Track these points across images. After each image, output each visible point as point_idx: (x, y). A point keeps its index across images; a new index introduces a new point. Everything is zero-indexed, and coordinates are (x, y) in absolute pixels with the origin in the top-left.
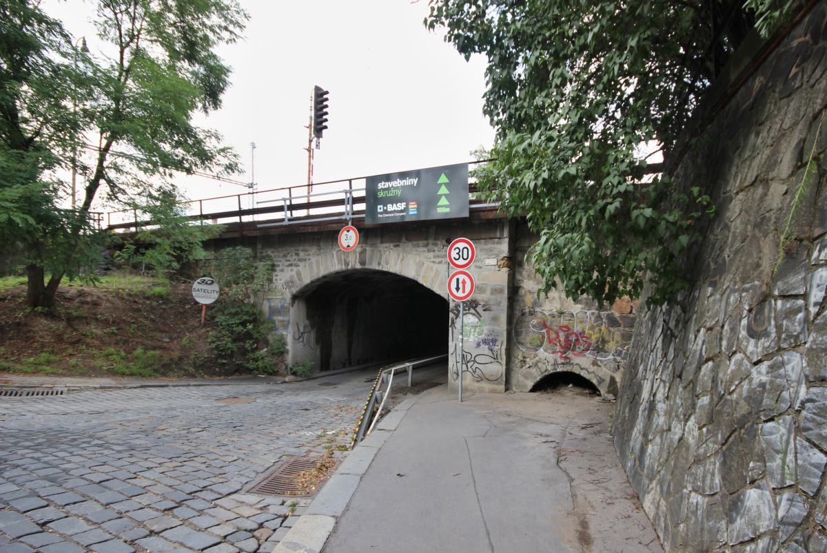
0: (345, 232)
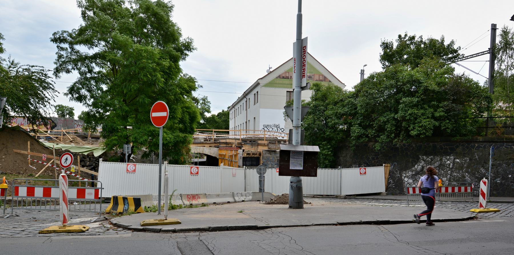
0: (107, 210)
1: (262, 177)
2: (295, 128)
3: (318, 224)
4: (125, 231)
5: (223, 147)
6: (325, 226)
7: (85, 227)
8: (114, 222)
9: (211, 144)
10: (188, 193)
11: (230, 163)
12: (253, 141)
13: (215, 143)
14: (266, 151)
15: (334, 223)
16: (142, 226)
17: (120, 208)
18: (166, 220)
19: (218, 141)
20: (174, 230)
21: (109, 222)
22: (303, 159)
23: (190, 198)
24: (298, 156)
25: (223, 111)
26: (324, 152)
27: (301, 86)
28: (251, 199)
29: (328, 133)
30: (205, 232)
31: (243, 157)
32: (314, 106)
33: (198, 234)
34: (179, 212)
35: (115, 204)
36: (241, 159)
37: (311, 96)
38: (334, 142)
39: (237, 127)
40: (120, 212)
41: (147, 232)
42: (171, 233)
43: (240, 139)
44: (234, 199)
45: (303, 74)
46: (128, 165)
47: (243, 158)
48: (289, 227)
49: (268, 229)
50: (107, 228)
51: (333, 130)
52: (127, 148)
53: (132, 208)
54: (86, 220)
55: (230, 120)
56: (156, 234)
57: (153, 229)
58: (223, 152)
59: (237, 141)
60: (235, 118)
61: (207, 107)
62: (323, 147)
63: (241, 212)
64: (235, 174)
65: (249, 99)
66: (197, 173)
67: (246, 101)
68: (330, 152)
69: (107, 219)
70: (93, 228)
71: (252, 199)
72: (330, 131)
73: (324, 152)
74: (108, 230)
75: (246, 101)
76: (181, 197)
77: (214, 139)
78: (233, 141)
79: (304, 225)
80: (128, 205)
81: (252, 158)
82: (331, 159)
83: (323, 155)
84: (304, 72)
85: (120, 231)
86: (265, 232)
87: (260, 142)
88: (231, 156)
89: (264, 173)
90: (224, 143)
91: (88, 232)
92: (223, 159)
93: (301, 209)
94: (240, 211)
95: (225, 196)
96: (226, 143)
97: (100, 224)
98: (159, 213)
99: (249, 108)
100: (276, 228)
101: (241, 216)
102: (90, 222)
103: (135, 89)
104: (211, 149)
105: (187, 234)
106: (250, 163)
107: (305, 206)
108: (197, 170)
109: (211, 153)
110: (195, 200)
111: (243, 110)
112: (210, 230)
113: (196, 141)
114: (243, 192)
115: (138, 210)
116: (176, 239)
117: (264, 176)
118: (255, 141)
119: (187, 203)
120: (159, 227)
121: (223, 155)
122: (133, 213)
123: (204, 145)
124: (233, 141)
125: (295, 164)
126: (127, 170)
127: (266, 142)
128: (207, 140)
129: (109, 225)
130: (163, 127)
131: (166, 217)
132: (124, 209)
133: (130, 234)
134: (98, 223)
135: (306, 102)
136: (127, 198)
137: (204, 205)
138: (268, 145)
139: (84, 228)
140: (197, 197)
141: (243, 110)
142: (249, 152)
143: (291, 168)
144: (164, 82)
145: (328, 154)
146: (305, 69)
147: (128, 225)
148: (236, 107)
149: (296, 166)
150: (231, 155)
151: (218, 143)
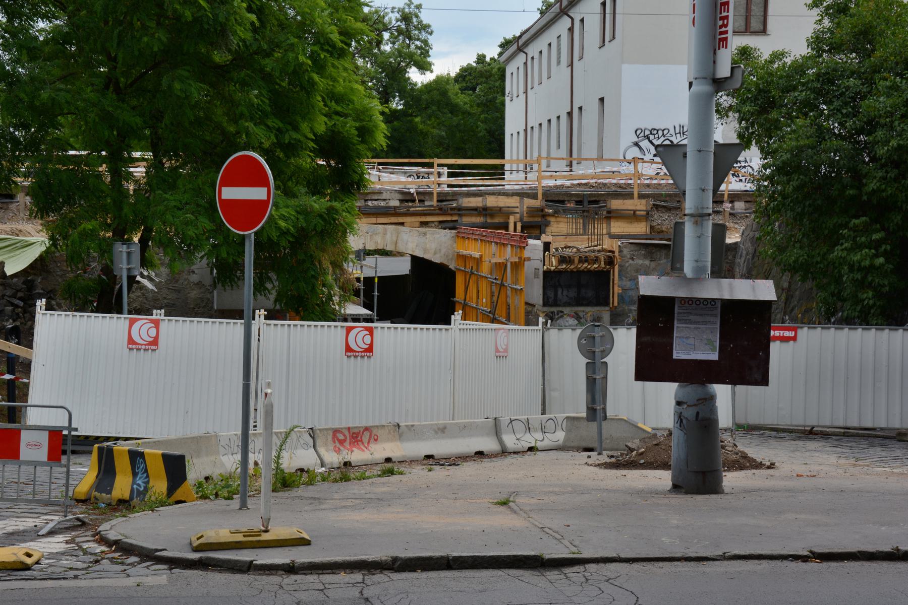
1: (598, 364)
2: (693, 219)
3: (743, 553)
4: (147, 567)
5: (474, 225)
6: (764, 562)
7: (30, 552)
8: (112, 536)
9: (425, 215)
10: (337, 426)
11: (495, 290)
12: (591, 202)
13: (441, 209)
14: (632, 247)
15: (800, 553)
16: (196, 550)
17: (122, 486)
18: (266, 531)
20: (288, 565)
21: (93, 536)
22: (718, 326)
23: (341, 442)
24: (701, 315)
25: (481, 59)
26: (856, 257)
27: (714, 74)
28: (561, 442)
29: (872, 185)
30: (381, 573)
31: (544, 272)
32: (818, 75)
33: (361, 580)
34: (306, 498)
35: (104, 471)
36: (536, 276)
37: (809, 33)
38: (897, 218)
39: (536, 130)
40: (121, 497)
41: (213, 571)
42: (281, 576)
43: (540, 196)
44: (501, 442)
45: (721, 33)
46: (132, 322)
47: (547, 274)
48: (645, 564)
49: (576, 568)
50: (91, 554)
51: (892, 174)
52: (125, 256)
53: (160, 485)
54: (22, 528)
55: (507, 99)
56: (238, 577)
57: (229, 561)
58: (473, 250)
59: (529, 202)
60: (526, 92)
61: (420, 48)
62: (855, 237)
63: (504, 503)
64: (506, 351)
65: (582, 21)
66: (370, 349)
67: (571, 30)
68: (881, 260)
69: (83, 524)
70: (50, 554)
71: (566, 440)
72: (880, 174)
73: (856, 257)
74: (97, 562)
75: (571, 30)
76: (313, 438)
77: (439, 194)
78: (513, 202)
79: (693, 555)
80: (148, 476)
81: (580, 273)
82: (884, 286)
83: (851, 268)
84: (724, 29)
85: (132, 565)
86: (562, 576)
87: (616, 204)
88: (502, 267)
89: (606, 353)
90: (475, 209)
91: (41, 570)
92: (472, 273)
93: (714, 496)
94: (502, 497)
95: (465, 430)
96: (484, 211)
97: (67, 542)
98: (243, 505)
99: (581, 58)
100: (602, 565)
101: (504, 520)
102: (34, 534)
103: (156, 49)
104: (425, 234)
105: (328, 578)
106: (573, 293)
107: (731, 479)
108: (368, 340)
109: (425, 251)
110: (360, 449)
111: (559, 63)
112: (396, 565)
113: (370, 203)
114: (536, 417)
115: (179, 494)
116: (297, 594)
117: (606, 363)
118: (596, 202)
119: (333, 458)
120: (244, 556)
121: (471, 257)
122: (163, 504)
123: (401, 220)
124: (513, 202)
125: (691, 341)
126: (131, 341)
127: (640, 205)
128: (413, 201)
129: (96, 545)
130: (256, 233)
131: (266, 522)
132: (132, 490)
133: (165, 577)
134: (60, 538)
135: (788, 60)
136: (141, 455)
137: (389, 467)
138: (647, 216)
139: (29, 555)
140: (367, 435)
141: (559, 63)
142: (568, 252)
143: (675, 356)
144: (253, 24)
145: (872, 266)
146: (727, 17)
147: (154, 547)
148: (532, 50)
149: (695, 349)
150: (500, 261)
151: (452, 209)
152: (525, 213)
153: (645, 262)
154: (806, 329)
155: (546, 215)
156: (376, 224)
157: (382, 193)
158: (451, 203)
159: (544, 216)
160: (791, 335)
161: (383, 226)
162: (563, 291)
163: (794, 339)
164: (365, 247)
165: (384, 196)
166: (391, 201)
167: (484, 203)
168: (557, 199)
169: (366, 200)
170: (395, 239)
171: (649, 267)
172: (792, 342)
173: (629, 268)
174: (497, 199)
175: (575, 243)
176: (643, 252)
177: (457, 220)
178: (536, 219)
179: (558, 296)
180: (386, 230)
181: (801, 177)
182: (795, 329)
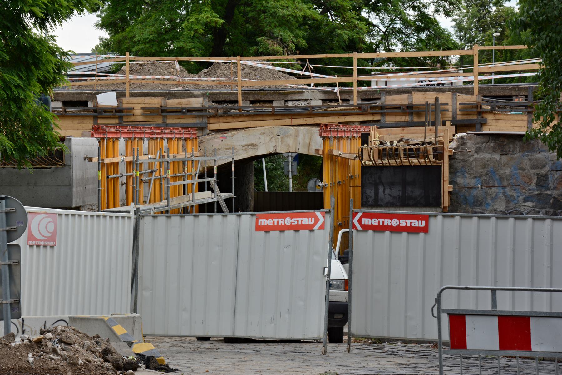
9: (344, 114)
14: (479, 139)
19: (378, 103)
43: (476, 91)
59: (463, 98)
90: (398, 107)
106: (396, 192)
113: (290, 104)
128: (337, 101)
152: (458, 110)
153: (494, 156)
154: (440, 218)
155: (483, 113)
156: (291, 126)
157: (303, 92)
158: (375, 102)
159: (480, 113)
160: (420, 225)
161: (295, 127)
162: (384, 189)
163: (425, 230)
164: (276, 150)
165: (305, 96)
166: (312, 101)
167: (410, 101)
168: (502, 94)
169: (286, 101)
170: (307, 141)
171: (500, 162)
172: (422, 234)
173: (474, 164)
174: (425, 96)
175: (414, 135)
176: (492, 145)
177: (380, 120)
178: (470, 117)
179: (380, 195)
180: (297, 131)
181: (550, 34)
182: (426, 218)
